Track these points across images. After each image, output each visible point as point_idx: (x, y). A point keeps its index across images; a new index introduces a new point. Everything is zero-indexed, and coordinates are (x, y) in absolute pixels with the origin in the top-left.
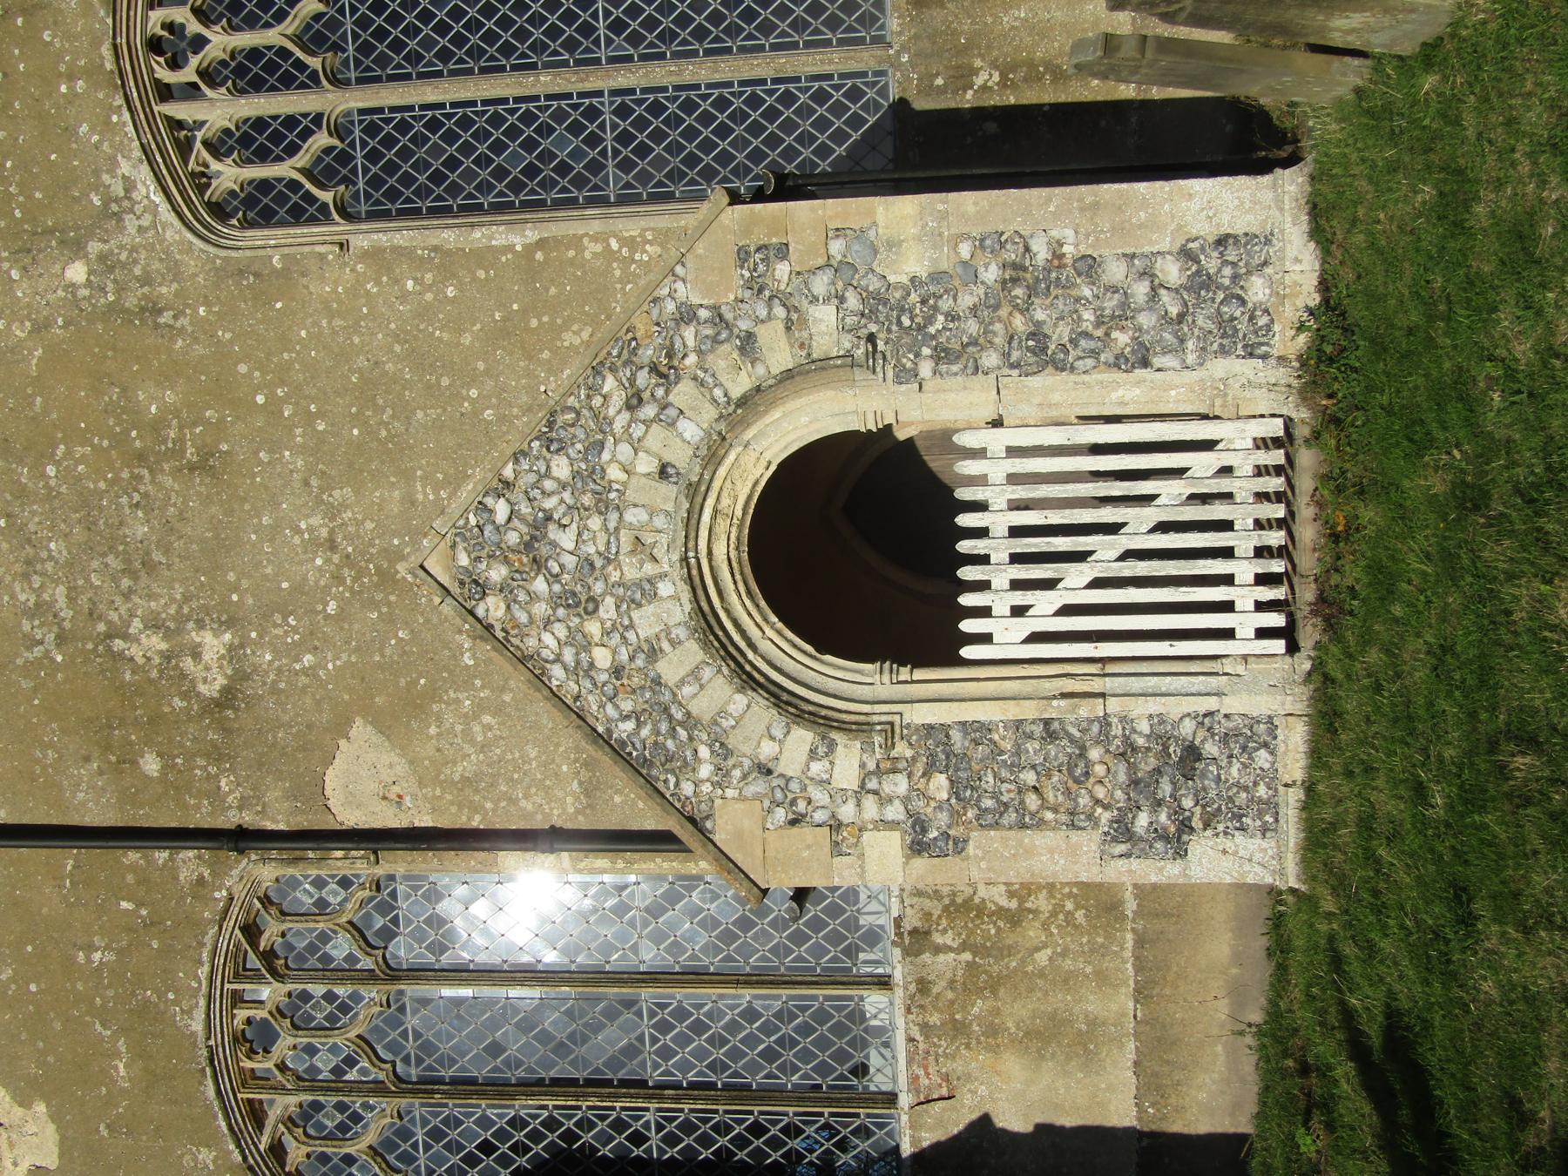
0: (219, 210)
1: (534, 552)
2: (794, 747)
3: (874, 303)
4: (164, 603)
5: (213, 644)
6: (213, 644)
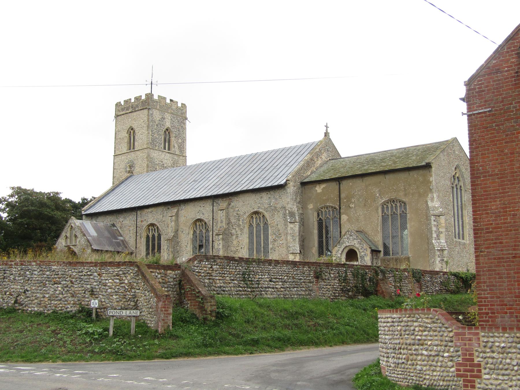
0: (383, 206)
1: (351, 236)
2: (340, 252)
3: (364, 257)
4: (356, 202)
5: (353, 206)
6: (353, 206)
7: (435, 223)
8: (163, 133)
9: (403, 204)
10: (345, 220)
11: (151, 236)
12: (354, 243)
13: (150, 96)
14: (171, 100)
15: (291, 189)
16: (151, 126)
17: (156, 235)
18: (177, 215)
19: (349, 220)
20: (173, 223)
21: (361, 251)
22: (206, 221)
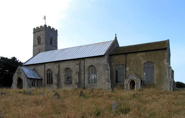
7: (168, 71)
10: (128, 69)
11: (49, 73)
12: (134, 78)
13: (45, 26)
14: (52, 28)
15: (106, 57)
16: (46, 37)
17: (51, 73)
20: (57, 69)
22: (71, 68)
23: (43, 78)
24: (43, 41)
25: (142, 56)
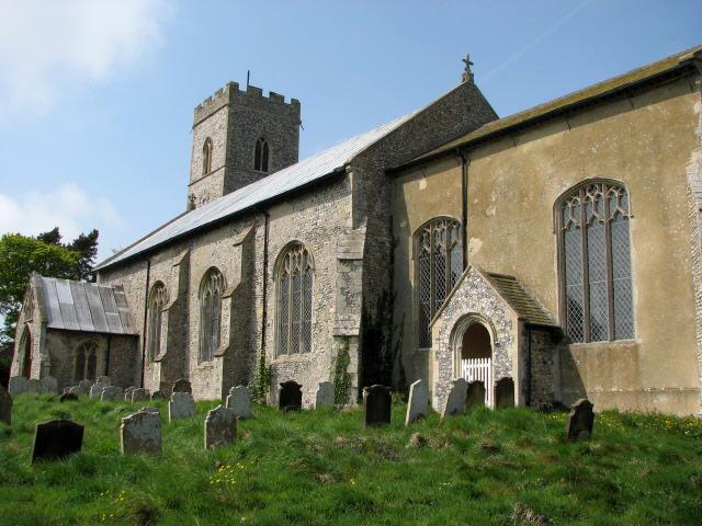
1: (473, 286)
5: (494, 212)
8: (254, 144)
9: (617, 194)
10: (476, 249)
14: (271, 93)
18: (250, 239)
19: (484, 251)
21: (498, 328)
23: (141, 334)
24: (219, 156)
25: (549, 151)
